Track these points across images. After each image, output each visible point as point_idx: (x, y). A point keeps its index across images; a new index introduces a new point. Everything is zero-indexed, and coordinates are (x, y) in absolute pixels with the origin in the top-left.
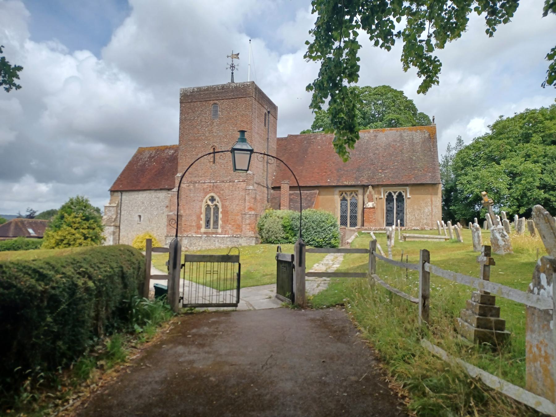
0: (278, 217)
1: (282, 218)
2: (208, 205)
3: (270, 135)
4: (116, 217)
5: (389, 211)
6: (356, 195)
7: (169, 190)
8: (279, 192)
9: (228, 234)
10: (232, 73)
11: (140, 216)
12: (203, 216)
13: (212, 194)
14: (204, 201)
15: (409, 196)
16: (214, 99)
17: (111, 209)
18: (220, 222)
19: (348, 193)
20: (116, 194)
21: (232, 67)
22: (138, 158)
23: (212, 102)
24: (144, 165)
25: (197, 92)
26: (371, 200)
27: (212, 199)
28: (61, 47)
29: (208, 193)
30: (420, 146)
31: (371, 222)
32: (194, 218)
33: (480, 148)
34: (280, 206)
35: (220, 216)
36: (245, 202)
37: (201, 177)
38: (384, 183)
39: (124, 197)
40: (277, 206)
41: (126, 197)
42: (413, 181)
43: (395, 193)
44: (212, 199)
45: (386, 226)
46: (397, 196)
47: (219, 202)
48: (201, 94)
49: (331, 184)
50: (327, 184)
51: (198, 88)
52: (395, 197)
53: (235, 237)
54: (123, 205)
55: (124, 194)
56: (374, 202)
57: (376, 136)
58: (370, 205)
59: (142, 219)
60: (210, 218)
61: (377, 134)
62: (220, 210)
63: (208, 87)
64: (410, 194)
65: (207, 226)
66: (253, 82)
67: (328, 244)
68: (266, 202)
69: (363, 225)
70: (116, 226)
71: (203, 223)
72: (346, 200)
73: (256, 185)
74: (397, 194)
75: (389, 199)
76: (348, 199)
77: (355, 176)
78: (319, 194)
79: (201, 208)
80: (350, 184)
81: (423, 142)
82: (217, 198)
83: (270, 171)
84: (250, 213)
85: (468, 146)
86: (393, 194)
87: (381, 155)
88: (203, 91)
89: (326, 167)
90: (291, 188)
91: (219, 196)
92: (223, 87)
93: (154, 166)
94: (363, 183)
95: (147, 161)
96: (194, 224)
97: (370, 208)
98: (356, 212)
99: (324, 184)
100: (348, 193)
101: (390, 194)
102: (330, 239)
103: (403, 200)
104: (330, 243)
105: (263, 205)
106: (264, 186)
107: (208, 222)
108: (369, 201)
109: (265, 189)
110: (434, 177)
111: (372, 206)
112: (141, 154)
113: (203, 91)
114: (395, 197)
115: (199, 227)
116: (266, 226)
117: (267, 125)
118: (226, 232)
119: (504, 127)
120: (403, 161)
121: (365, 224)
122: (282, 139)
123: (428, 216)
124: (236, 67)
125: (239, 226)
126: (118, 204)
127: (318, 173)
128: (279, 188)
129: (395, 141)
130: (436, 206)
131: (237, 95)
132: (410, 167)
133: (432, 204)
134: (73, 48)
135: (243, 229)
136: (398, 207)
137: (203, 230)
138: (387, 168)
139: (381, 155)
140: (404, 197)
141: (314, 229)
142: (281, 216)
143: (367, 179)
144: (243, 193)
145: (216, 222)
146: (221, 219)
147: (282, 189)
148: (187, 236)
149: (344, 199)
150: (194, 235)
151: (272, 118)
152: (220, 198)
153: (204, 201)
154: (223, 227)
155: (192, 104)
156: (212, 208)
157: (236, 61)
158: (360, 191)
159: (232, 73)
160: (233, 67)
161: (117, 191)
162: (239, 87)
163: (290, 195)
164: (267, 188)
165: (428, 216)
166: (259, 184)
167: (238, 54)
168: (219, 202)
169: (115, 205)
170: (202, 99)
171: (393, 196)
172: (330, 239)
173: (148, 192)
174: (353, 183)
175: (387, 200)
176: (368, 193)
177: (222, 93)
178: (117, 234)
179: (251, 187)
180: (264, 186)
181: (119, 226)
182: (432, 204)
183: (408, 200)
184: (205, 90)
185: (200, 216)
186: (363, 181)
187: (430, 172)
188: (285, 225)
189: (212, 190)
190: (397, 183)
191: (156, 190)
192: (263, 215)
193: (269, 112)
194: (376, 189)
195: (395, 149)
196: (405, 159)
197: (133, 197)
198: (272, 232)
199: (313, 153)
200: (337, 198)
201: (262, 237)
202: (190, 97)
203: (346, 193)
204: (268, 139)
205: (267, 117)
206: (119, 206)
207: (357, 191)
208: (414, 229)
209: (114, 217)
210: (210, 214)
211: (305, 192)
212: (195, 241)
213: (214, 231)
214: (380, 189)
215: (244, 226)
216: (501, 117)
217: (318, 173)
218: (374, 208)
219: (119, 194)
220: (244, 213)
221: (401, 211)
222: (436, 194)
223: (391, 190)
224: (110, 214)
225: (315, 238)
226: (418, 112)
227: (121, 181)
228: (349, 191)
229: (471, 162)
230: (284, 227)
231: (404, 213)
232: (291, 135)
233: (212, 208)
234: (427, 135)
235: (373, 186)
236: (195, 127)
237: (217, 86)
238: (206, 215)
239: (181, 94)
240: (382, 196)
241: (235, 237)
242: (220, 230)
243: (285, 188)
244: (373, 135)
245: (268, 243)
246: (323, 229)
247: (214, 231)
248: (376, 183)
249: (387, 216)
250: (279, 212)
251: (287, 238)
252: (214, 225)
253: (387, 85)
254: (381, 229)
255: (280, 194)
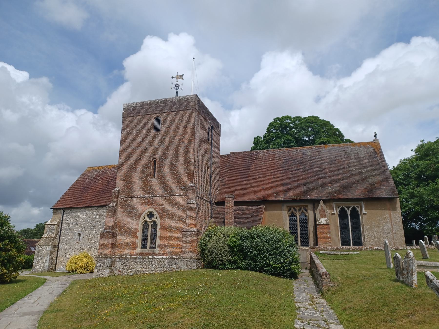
0: (224, 235)
1: (228, 236)
2: (146, 222)
3: (213, 149)
4: (56, 236)
5: (344, 228)
6: (306, 210)
7: (105, 206)
8: (222, 207)
9: (166, 255)
10: (177, 92)
11: (79, 235)
12: (140, 234)
13: (151, 209)
14: (142, 217)
15: (364, 212)
16: (157, 112)
17: (52, 227)
18: (158, 241)
19: (297, 209)
20: (58, 211)
21: (177, 86)
22: (85, 176)
23: (154, 116)
24: (90, 183)
25: (139, 106)
26: (323, 215)
27: (151, 215)
28: (67, 107)
29: (144, 209)
30: (367, 160)
31: (326, 240)
32: (130, 236)
33: (408, 169)
34: (224, 222)
35: (158, 233)
36: (186, 218)
37: (140, 191)
38: (337, 198)
39: (65, 215)
40: (221, 222)
41: (69, 216)
42: (368, 195)
43: (348, 208)
44: (151, 215)
45: (342, 245)
46: (351, 211)
47: (158, 218)
48: (143, 108)
49: (278, 199)
50: (274, 199)
51: (141, 103)
52: (349, 213)
53: (174, 258)
54: (64, 223)
55: (66, 211)
56: (327, 219)
57: (318, 152)
58: (323, 221)
59: (81, 237)
60: (147, 236)
61: (320, 150)
62: (159, 227)
63: (151, 101)
64: (365, 209)
65: (144, 245)
66: (197, 95)
67: (287, 270)
68: (210, 219)
69: (316, 244)
70: (55, 246)
71: (139, 242)
72: (296, 216)
73: (198, 200)
74: (350, 209)
75: (343, 215)
76: (298, 215)
77: (302, 190)
78: (266, 210)
79: (138, 225)
80: (298, 198)
81: (369, 157)
82: (156, 214)
83: (213, 185)
84: (191, 230)
85: (397, 167)
86: (346, 209)
87: (327, 169)
88: (146, 105)
89: (271, 182)
90: (237, 203)
91: (157, 211)
92: (166, 101)
93: (100, 183)
94: (313, 198)
95: (94, 179)
96: (129, 243)
97: (324, 225)
98: (307, 229)
99: (270, 199)
100: (297, 209)
101: (343, 209)
102: (290, 263)
103: (358, 215)
104: (290, 269)
105: (206, 221)
106: (207, 201)
107: (144, 241)
108: (322, 217)
109: (208, 204)
110: (389, 190)
111: (325, 223)
112: (89, 173)
113: (146, 105)
114: (349, 213)
115: (135, 248)
116: (209, 246)
117: (210, 140)
118: (162, 253)
119: (428, 149)
120: (352, 175)
121: (319, 243)
122: (225, 156)
123: (389, 233)
124: (180, 87)
125: (179, 245)
126: (59, 222)
127: (263, 188)
128: (221, 204)
129: (339, 156)
130: (396, 223)
131: (180, 108)
132: (361, 181)
133: (391, 220)
134: (74, 108)
135: (183, 249)
136: (353, 223)
137: (139, 250)
138: (336, 182)
139: (327, 169)
140: (359, 213)
141: (269, 251)
142: (227, 234)
143: (317, 193)
144: (184, 208)
145: (153, 241)
146: (159, 229)
147: (226, 204)
148: (121, 258)
149: (292, 216)
150: (129, 257)
151: (215, 134)
152: (159, 213)
153: (142, 217)
154: (160, 246)
155: (134, 118)
156: (150, 224)
157: (180, 81)
158: (310, 206)
159: (177, 92)
160: (177, 86)
161: (60, 209)
162: (182, 100)
163: (235, 210)
164: (211, 202)
165: (389, 233)
166: (201, 198)
167: (183, 75)
168: (158, 218)
169: (56, 223)
170: (145, 113)
171: (346, 212)
172: (290, 263)
173: (90, 209)
174: (302, 197)
175: (340, 216)
176: (319, 208)
177: (164, 106)
178: (55, 254)
179: (193, 201)
180: (207, 201)
181: (58, 245)
182: (391, 220)
183: (364, 216)
184: (148, 105)
185: (136, 235)
186: (312, 195)
187: (384, 186)
188: (232, 245)
189: (151, 206)
190: (350, 197)
191: (98, 207)
192: (206, 232)
193: (212, 127)
194: (328, 204)
195: (341, 164)
196: (354, 173)
197: (75, 214)
198: (217, 254)
199: (256, 169)
200: (285, 214)
201: (204, 260)
202: (133, 112)
203: (294, 209)
204: (211, 153)
205: (210, 131)
206: (61, 223)
207: (307, 206)
208: (377, 249)
209: (54, 235)
210: (148, 231)
211: (251, 207)
212: (130, 263)
213: (151, 251)
214: (331, 204)
215: (184, 245)
216: (422, 141)
217: (263, 188)
218: (328, 224)
219: (62, 211)
220: (184, 230)
221: (357, 228)
222: (395, 209)
223: (343, 205)
224: (50, 232)
225: (271, 263)
226: (345, 138)
227: (65, 199)
228: (298, 206)
229: (402, 182)
230: (230, 247)
231: (360, 231)
232: (234, 153)
233: (150, 224)
234: (372, 150)
235: (325, 201)
236: (137, 140)
237: (160, 101)
238: (143, 233)
239: (124, 109)
240: (335, 212)
241: (174, 258)
242: (157, 251)
243: (230, 203)
244: (316, 151)
245: (211, 268)
246: (280, 250)
247: (151, 251)
248: (327, 198)
249: (342, 234)
250: (225, 229)
251: (235, 262)
252: (151, 244)
253: (316, 116)
254: (336, 250)
255: (225, 209)
